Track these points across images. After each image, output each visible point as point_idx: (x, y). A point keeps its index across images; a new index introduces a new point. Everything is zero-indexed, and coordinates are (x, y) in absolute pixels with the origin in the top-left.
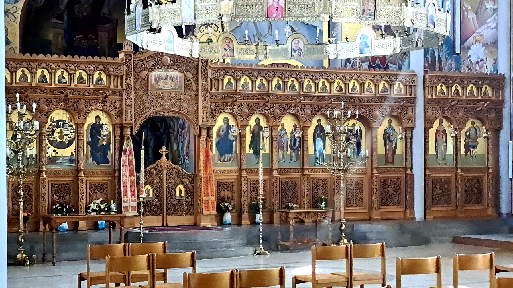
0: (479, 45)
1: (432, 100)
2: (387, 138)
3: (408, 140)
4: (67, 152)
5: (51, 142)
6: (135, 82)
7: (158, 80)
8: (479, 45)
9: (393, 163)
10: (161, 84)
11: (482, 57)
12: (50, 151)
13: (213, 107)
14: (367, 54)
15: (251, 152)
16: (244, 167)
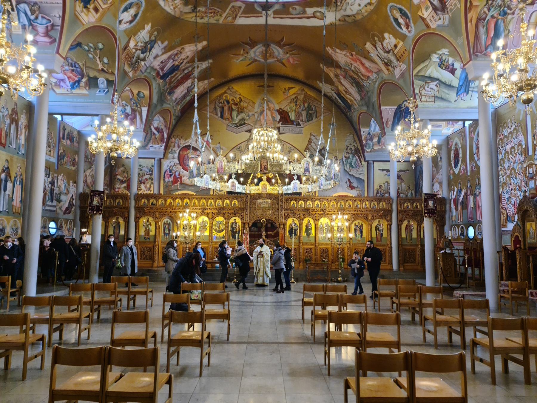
0: (437, 183)
1: (401, 211)
2: (377, 229)
3: (390, 230)
4: (221, 234)
5: (215, 230)
6: (250, 204)
7: (260, 203)
8: (437, 183)
9: (381, 241)
10: (262, 205)
11: (438, 189)
12: (215, 233)
13: (286, 215)
14: (152, 65)
15: (306, 235)
16: (301, 242)
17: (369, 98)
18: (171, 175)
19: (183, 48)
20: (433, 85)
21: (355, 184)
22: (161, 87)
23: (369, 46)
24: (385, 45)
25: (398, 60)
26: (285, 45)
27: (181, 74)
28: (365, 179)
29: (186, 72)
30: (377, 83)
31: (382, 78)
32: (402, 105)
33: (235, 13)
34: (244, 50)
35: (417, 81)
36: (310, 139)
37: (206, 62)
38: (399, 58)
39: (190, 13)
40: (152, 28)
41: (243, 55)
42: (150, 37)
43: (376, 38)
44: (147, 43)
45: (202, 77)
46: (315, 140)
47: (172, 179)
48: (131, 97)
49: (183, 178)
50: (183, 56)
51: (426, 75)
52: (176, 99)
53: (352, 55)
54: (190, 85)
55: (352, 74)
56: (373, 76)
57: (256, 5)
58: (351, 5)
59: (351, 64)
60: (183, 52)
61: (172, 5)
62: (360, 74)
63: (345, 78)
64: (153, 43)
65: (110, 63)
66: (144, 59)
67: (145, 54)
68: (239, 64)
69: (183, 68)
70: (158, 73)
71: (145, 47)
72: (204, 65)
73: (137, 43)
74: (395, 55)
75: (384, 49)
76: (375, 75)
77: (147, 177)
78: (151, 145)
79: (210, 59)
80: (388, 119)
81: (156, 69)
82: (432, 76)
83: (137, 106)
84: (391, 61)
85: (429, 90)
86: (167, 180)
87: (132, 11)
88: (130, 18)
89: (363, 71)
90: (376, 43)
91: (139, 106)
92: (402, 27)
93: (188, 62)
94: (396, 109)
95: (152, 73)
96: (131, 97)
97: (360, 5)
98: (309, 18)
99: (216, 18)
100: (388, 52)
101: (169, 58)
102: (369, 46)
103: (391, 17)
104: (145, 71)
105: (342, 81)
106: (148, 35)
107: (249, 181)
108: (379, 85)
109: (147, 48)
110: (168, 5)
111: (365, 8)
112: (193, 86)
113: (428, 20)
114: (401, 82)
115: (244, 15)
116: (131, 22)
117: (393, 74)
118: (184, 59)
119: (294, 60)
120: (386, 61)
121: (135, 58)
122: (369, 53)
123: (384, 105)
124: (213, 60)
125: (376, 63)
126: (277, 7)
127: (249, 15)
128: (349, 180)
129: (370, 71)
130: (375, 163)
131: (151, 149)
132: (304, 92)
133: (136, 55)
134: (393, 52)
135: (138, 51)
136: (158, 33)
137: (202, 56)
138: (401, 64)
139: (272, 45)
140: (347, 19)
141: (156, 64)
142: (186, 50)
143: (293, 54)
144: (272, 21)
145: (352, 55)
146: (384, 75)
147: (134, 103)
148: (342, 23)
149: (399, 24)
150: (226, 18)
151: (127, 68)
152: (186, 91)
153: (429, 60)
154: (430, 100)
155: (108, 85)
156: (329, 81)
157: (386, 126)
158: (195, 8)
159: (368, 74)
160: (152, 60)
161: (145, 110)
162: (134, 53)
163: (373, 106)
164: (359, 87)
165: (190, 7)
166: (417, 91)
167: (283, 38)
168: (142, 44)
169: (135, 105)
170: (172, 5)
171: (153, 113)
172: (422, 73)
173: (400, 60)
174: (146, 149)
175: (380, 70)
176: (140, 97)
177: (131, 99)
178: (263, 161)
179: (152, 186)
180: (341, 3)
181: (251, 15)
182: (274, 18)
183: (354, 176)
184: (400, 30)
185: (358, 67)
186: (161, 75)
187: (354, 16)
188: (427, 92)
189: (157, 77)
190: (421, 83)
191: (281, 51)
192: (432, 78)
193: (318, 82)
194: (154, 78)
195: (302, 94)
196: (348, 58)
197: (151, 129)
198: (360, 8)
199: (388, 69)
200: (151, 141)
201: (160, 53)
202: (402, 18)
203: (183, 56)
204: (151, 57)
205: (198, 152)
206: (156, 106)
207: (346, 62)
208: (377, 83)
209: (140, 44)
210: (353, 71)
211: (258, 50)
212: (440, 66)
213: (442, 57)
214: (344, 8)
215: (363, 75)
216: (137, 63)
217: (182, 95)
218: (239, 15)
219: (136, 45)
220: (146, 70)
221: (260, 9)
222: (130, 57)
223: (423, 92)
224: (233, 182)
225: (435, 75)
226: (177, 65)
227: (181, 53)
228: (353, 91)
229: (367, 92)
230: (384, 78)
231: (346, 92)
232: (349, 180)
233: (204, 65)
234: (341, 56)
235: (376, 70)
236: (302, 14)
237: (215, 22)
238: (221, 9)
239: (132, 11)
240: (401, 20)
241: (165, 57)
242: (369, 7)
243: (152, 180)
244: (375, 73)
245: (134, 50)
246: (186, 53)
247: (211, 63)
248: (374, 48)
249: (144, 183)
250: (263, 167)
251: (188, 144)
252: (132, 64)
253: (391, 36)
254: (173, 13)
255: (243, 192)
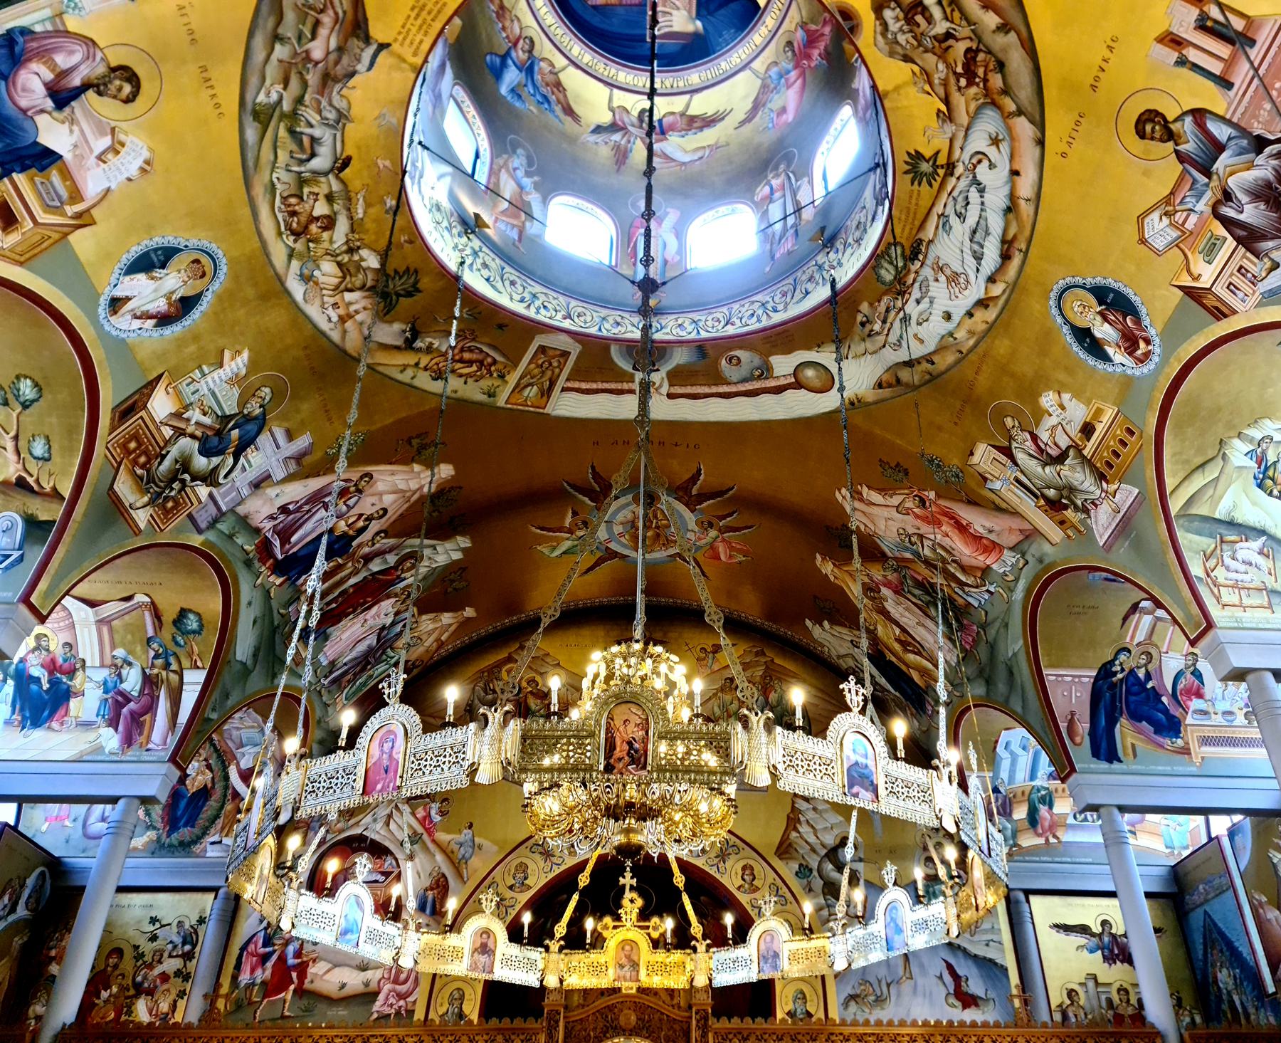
14: (241, 510)
17: (992, 647)
18: (264, 959)
19: (369, 475)
20: (1249, 549)
21: (975, 986)
22: (274, 604)
23: (983, 456)
24: (1044, 436)
25: (1102, 477)
26: (702, 497)
27: (356, 572)
28: (1010, 962)
29: (376, 566)
30: (1022, 585)
31: (1041, 561)
32: (1112, 663)
33: (549, 373)
34: (575, 514)
35: (1191, 536)
36: (793, 807)
37: (449, 545)
38: (1104, 469)
39: (397, 348)
40: (253, 366)
41: (571, 531)
42: (242, 402)
43: (1009, 422)
44: (225, 419)
45: (436, 596)
46: (811, 815)
47: (268, 973)
48: (150, 633)
49: (312, 970)
50: (367, 505)
51: (1217, 516)
52: (332, 663)
53: (922, 502)
54: (389, 620)
55: (923, 571)
56: (1004, 564)
57: (614, 350)
58: (919, 324)
59: (921, 537)
60: (368, 491)
61: (335, 305)
62: (952, 568)
63: (898, 591)
64: (251, 427)
65: (56, 457)
66: (210, 478)
67: (215, 460)
68: (561, 564)
69: (366, 550)
70: (265, 548)
71: (218, 433)
72: (445, 553)
73: (187, 407)
74: (1087, 462)
75: (1041, 451)
76: (1010, 558)
77: (171, 965)
78: (216, 838)
79: (463, 534)
80: (1073, 714)
81: (258, 531)
82: (1240, 517)
83: (167, 666)
84: (1072, 489)
85: (1243, 568)
86: (245, 978)
87: (173, 281)
88: (161, 305)
89: (964, 550)
90: (1011, 439)
91: (174, 667)
92: (1110, 351)
93: (386, 533)
94: (1097, 679)
95: (240, 540)
96: (150, 633)
97: (948, 316)
98: (778, 390)
99: (486, 383)
100: (1061, 459)
101: (317, 499)
102: (983, 456)
103: (1066, 329)
104: (212, 524)
105: (890, 606)
106: (236, 392)
107: (561, 929)
108: (1028, 591)
109: (229, 436)
110: (318, 302)
111: (969, 322)
112: (398, 628)
113: (1220, 290)
114: (1121, 559)
115: (576, 385)
116: (164, 320)
117: (1085, 534)
118: (370, 519)
119: (732, 548)
120: (1051, 493)
121: (167, 463)
122: (985, 479)
123: (1051, 666)
124: (473, 541)
125: (1015, 513)
126: (680, 357)
127: (594, 386)
128: (950, 967)
129: (992, 547)
130: (1033, 899)
131: (213, 852)
132: (763, 660)
133: (174, 451)
134: (1079, 451)
135: (184, 442)
136: (277, 395)
137: (433, 516)
138: (1113, 487)
139: (664, 498)
140: (905, 375)
141: (261, 509)
142: (380, 486)
143: (730, 529)
144: (663, 409)
145: (922, 502)
146: (1047, 548)
147: (157, 656)
148: (886, 392)
149: (1095, 348)
150: (519, 388)
151: (125, 488)
152: (372, 640)
153: (1220, 462)
154: (1257, 602)
155: (26, 537)
156: (844, 614)
157: (1072, 740)
158: (415, 334)
159: (981, 560)
160: (245, 491)
161: (194, 681)
162: (167, 442)
163: (1011, 673)
164: (958, 617)
165: (397, 327)
166: (1196, 570)
167: (699, 470)
168: (207, 420)
169: (159, 662)
170: (335, 305)
171: (227, 696)
172: (1202, 509)
173: (1109, 473)
174: (189, 854)
175: (1032, 534)
176: (185, 633)
177: (149, 640)
178: (621, 713)
179: (181, 1004)
180: (884, 322)
181: (600, 386)
182: (671, 396)
183: (965, 951)
184: (1100, 365)
185: (946, 542)
186: (280, 557)
187: (928, 359)
188: (1234, 575)
189: (263, 561)
190: (1207, 543)
191: (690, 518)
192: (1240, 525)
193: (808, 623)
194: (248, 564)
195: (757, 664)
196: (910, 518)
197: (226, 778)
198: (950, 326)
199: (1062, 523)
200: (220, 822)
201: (279, 474)
202: (1105, 319)
203: (367, 505)
204: (241, 479)
205: (389, 860)
206: (246, 671)
207: (903, 533)
208: (1022, 585)
209: (195, 415)
210: (927, 562)
211: (620, 517)
212: (1260, 486)
213: (1264, 453)
214: (893, 338)
215: (963, 569)
216: (176, 485)
217: (354, 654)
218: (561, 383)
219: (177, 415)
220: (216, 521)
221: (626, 366)
222: (146, 453)
223: (1220, 574)
224: (487, 932)
225: (1247, 515)
226: (345, 534)
227: (360, 491)
228: (933, 635)
229: (984, 626)
230: (1047, 561)
231: (904, 644)
232: (950, 967)
233: (445, 553)
234: (883, 516)
235: (1014, 539)
236: (759, 377)
237: (483, 398)
238: (504, 355)
239: (173, 281)
240: (1103, 331)
241: (297, 491)
242: (980, 315)
243: (186, 977)
244: (1011, 549)
245: (167, 432)
246: (381, 494)
247: (464, 550)
248: (1003, 458)
249: (150, 992)
250: (621, 750)
251: (358, 831)
252: (151, 480)
253: (1066, 397)
254: (335, 336)
255: (531, 980)
